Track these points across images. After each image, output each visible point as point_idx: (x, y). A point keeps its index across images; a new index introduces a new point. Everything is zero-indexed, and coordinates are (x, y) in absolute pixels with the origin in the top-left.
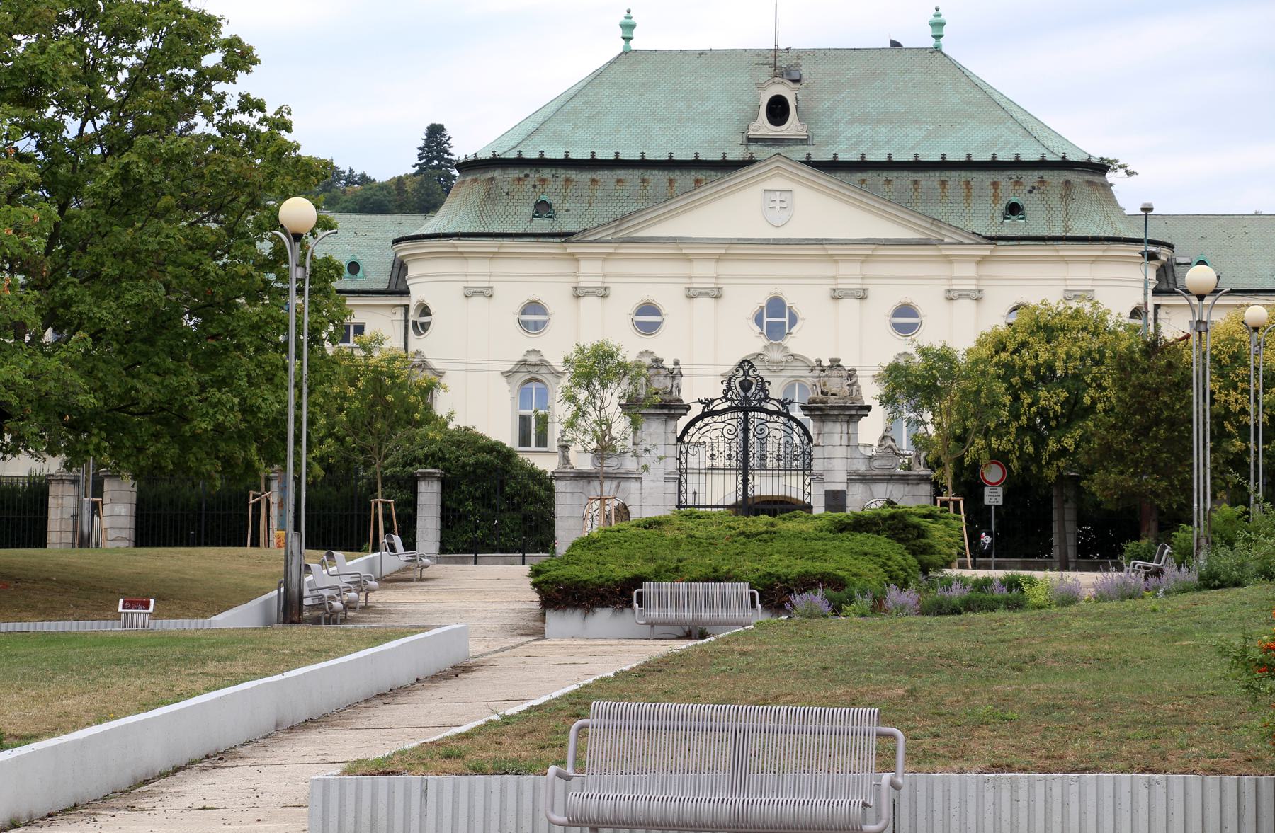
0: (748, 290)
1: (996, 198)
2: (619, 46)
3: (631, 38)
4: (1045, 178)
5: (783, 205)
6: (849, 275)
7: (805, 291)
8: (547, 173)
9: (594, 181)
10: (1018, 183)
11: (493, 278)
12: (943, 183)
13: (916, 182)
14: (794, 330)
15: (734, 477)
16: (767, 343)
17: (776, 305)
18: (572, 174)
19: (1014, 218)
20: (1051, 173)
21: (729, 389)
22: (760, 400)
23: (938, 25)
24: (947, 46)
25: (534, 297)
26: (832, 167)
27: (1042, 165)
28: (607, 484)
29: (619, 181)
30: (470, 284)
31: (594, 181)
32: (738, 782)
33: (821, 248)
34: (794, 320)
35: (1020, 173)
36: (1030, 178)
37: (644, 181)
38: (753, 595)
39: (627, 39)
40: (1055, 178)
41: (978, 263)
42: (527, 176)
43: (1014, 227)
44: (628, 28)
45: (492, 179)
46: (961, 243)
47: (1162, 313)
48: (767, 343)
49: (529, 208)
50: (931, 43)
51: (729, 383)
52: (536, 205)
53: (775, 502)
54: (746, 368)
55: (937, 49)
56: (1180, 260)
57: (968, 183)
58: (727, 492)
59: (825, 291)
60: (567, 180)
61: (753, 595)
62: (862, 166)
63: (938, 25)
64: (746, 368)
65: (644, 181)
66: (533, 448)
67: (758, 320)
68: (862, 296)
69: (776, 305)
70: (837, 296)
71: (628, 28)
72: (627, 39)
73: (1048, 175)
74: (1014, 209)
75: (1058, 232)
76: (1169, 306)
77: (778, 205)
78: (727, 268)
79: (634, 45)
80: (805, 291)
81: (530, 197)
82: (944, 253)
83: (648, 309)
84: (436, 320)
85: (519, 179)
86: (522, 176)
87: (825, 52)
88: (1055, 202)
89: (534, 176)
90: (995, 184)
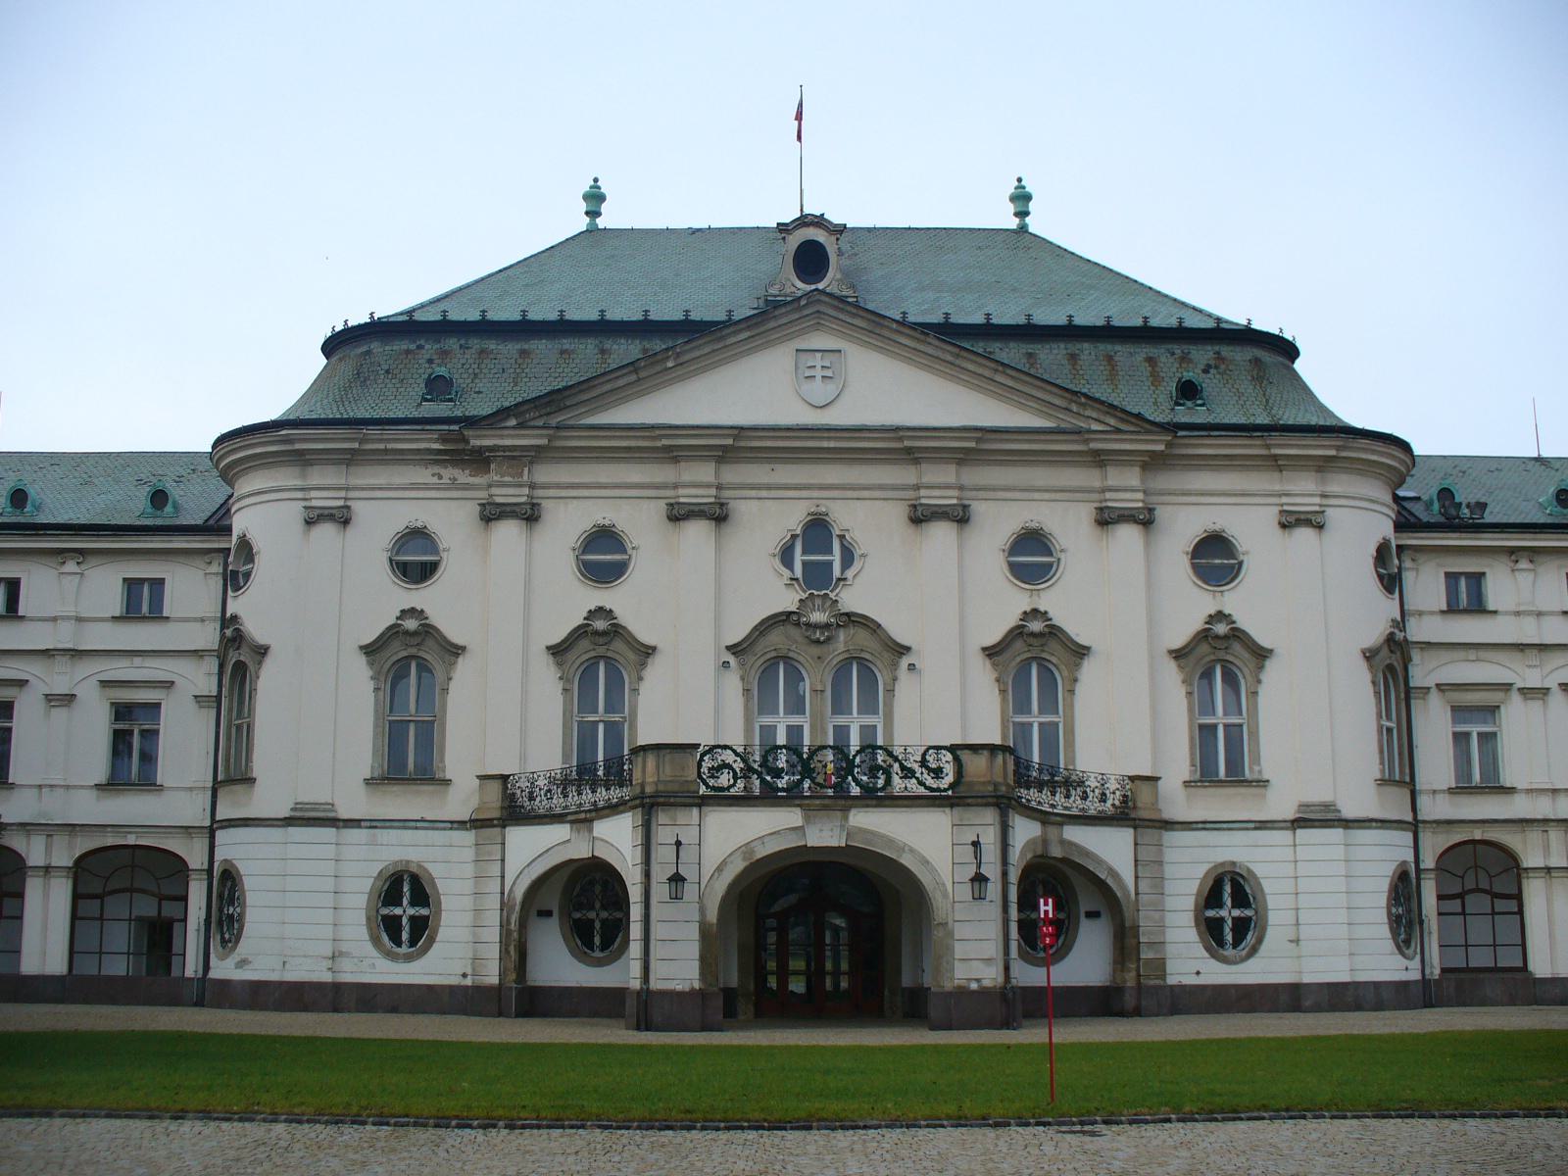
1: (1156, 379)
2: (582, 223)
4: (1224, 354)
5: (829, 373)
6: (939, 483)
8: (452, 343)
9: (524, 353)
11: (351, 494)
12: (1073, 358)
13: (1030, 355)
14: (849, 574)
17: (817, 531)
19: (1189, 404)
20: (1231, 348)
23: (1021, 199)
24: (1034, 225)
29: (562, 352)
30: (314, 503)
31: (524, 353)
33: (904, 446)
39: (593, 214)
40: (1240, 355)
41: (1145, 467)
42: (420, 347)
44: (595, 199)
45: (368, 352)
46: (1118, 431)
49: (420, 389)
50: (1013, 223)
53: (1210, 339)
55: (1023, 229)
57: (1110, 358)
59: (1271, 515)
60: (482, 352)
63: (1021, 199)
65: (603, 352)
67: (786, 556)
68: (960, 517)
69: (817, 531)
70: (920, 517)
71: (595, 199)
72: (593, 214)
74: (1188, 391)
77: (819, 373)
78: (733, 474)
79: (601, 222)
81: (419, 374)
85: (408, 352)
86: (413, 347)
88: (1247, 387)
89: (430, 348)
90: (1150, 360)
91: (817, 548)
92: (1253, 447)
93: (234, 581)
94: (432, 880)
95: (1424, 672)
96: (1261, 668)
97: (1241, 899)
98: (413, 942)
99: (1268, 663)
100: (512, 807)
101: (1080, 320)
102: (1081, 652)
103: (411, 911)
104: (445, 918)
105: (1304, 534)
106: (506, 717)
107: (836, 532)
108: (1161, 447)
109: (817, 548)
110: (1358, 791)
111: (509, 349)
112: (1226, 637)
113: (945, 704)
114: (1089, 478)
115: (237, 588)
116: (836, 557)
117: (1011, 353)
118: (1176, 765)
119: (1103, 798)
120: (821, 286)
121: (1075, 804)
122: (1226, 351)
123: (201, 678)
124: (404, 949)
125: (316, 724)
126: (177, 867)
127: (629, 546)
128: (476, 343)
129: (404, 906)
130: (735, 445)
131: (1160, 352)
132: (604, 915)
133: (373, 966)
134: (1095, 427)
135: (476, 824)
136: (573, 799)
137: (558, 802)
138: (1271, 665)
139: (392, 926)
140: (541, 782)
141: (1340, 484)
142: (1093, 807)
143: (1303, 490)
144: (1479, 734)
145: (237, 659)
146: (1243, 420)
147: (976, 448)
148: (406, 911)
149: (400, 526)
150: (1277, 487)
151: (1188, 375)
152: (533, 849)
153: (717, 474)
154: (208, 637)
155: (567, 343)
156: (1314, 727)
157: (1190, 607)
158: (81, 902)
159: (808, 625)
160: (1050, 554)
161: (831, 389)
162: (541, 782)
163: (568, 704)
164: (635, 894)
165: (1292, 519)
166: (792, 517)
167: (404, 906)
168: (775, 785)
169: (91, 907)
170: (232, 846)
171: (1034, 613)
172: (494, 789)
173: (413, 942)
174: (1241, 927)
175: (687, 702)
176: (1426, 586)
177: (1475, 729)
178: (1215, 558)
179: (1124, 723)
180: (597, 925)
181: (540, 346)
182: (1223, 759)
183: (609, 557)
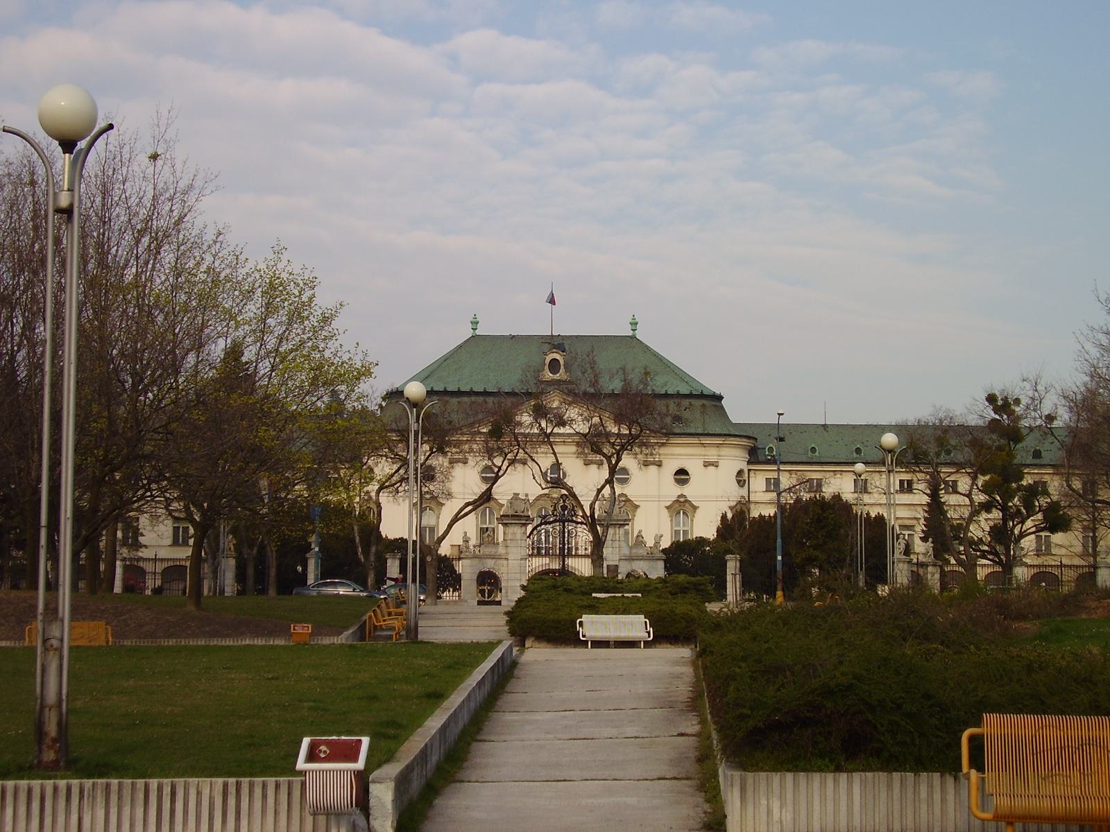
2: (470, 333)
3: (476, 329)
4: (693, 403)
15: (558, 560)
21: (555, 510)
22: (572, 516)
25: (681, 467)
27: (690, 396)
28: (583, 554)
32: (211, 781)
36: (686, 402)
38: (646, 622)
44: (475, 323)
47: (752, 474)
50: (630, 333)
51: (555, 507)
54: (564, 498)
56: (760, 446)
58: (541, 564)
59: (701, 463)
61: (646, 622)
64: (564, 498)
71: (475, 323)
73: (694, 402)
75: (700, 431)
79: (478, 332)
82: (702, 442)
87: (577, 337)
92: (695, 440)
96: (695, 512)
99: (697, 511)
102: (695, 508)
105: (711, 468)
112: (684, 502)
114: (701, 451)
127: (630, 473)
132: (489, 588)
138: (638, 510)
141: (725, 451)
143: (712, 454)
144: (908, 535)
150: (704, 453)
157: (672, 491)
159: (552, 497)
160: (628, 475)
163: (477, 521)
165: (707, 464)
168: (101, 553)
171: (682, 496)
178: (682, 475)
180: (487, 591)
183: (683, 477)
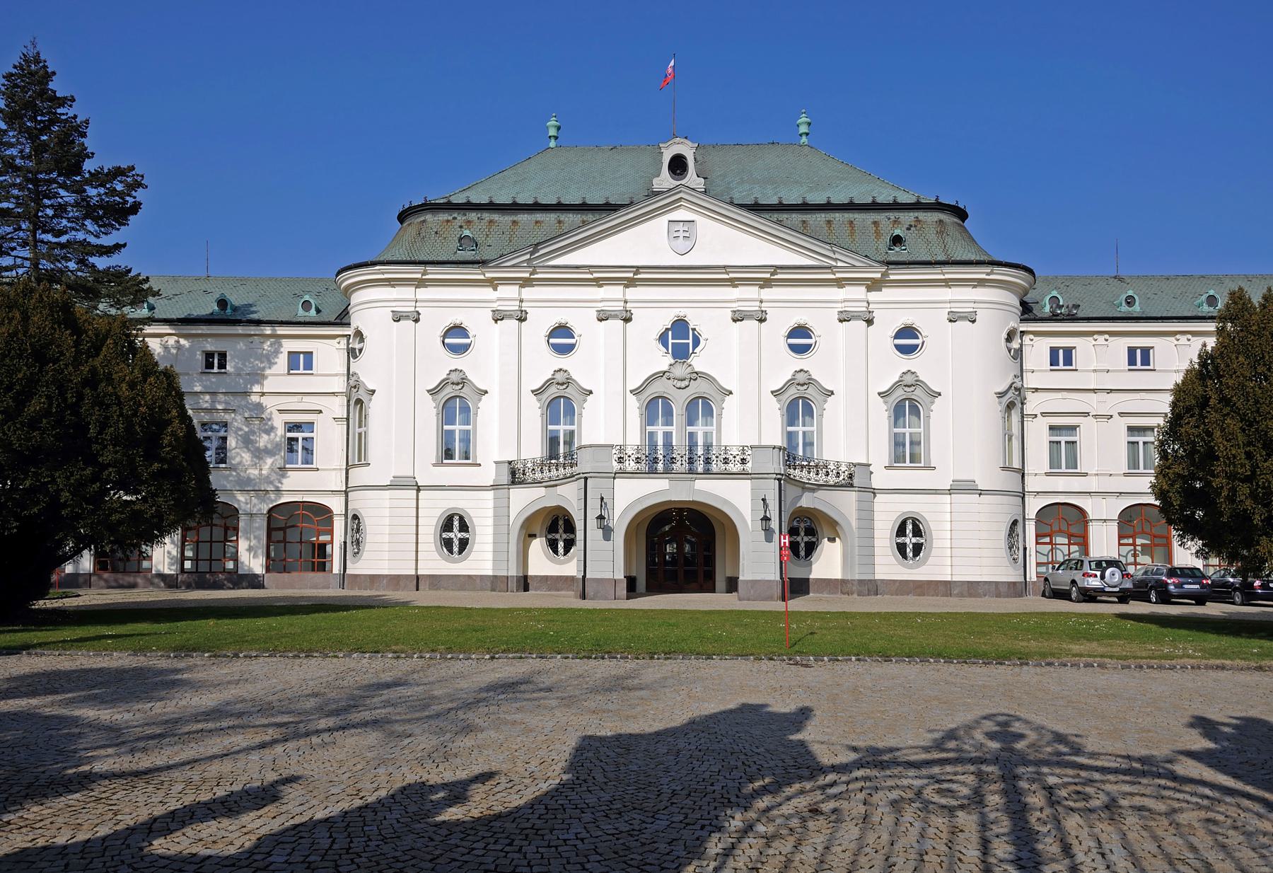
0: (655, 310)
1: (878, 234)
6: (747, 295)
7: (708, 312)
8: (473, 216)
10: (896, 222)
13: (829, 222)
16: (673, 361)
17: (680, 326)
18: (496, 217)
19: (897, 249)
26: (756, 208)
33: (729, 276)
34: (697, 342)
35: (897, 214)
37: (560, 222)
43: (897, 253)
48: (673, 361)
52: (460, 239)
62: (781, 208)
66: (457, 461)
69: (680, 326)
74: (897, 240)
75: (941, 258)
76: (1036, 334)
77: (681, 234)
78: (634, 293)
80: (708, 312)
83: (563, 330)
84: (368, 345)
85: (448, 221)
89: (460, 218)
90: (875, 223)
91: (680, 339)
93: (352, 353)
94: (470, 518)
95: (1034, 403)
97: (917, 532)
98: (460, 552)
100: (516, 476)
101: (834, 200)
103: (459, 535)
104: (478, 539)
106: (507, 429)
107: (691, 326)
108: (879, 275)
109: (680, 339)
110: (987, 473)
111: (504, 219)
113: (748, 424)
115: (355, 357)
116: (690, 341)
117: (796, 218)
118: (879, 454)
119: (838, 475)
120: (683, 182)
121: (822, 478)
122: (922, 215)
123: (337, 407)
124: (456, 556)
125: (403, 432)
126: (323, 513)
128: (487, 216)
129: (455, 532)
130: (634, 277)
131: (881, 217)
133: (434, 563)
134: (840, 264)
135: (495, 487)
136: (546, 474)
137: (538, 476)
139: (448, 544)
140: (529, 465)
142: (832, 480)
145: (357, 401)
146: (929, 259)
147: (770, 277)
148: (456, 535)
149: (448, 322)
151: (897, 232)
152: (524, 500)
153: (624, 294)
154: (340, 385)
155: (539, 216)
156: (962, 436)
158: (274, 533)
161: (689, 244)
162: (529, 465)
164: (579, 526)
166: (665, 319)
167: (455, 532)
169: (278, 535)
170: (360, 502)
172: (505, 470)
173: (460, 552)
174: (917, 549)
175: (608, 423)
176: (1037, 351)
177: (1063, 439)
179: (850, 433)
181: (523, 218)
182: (906, 452)
